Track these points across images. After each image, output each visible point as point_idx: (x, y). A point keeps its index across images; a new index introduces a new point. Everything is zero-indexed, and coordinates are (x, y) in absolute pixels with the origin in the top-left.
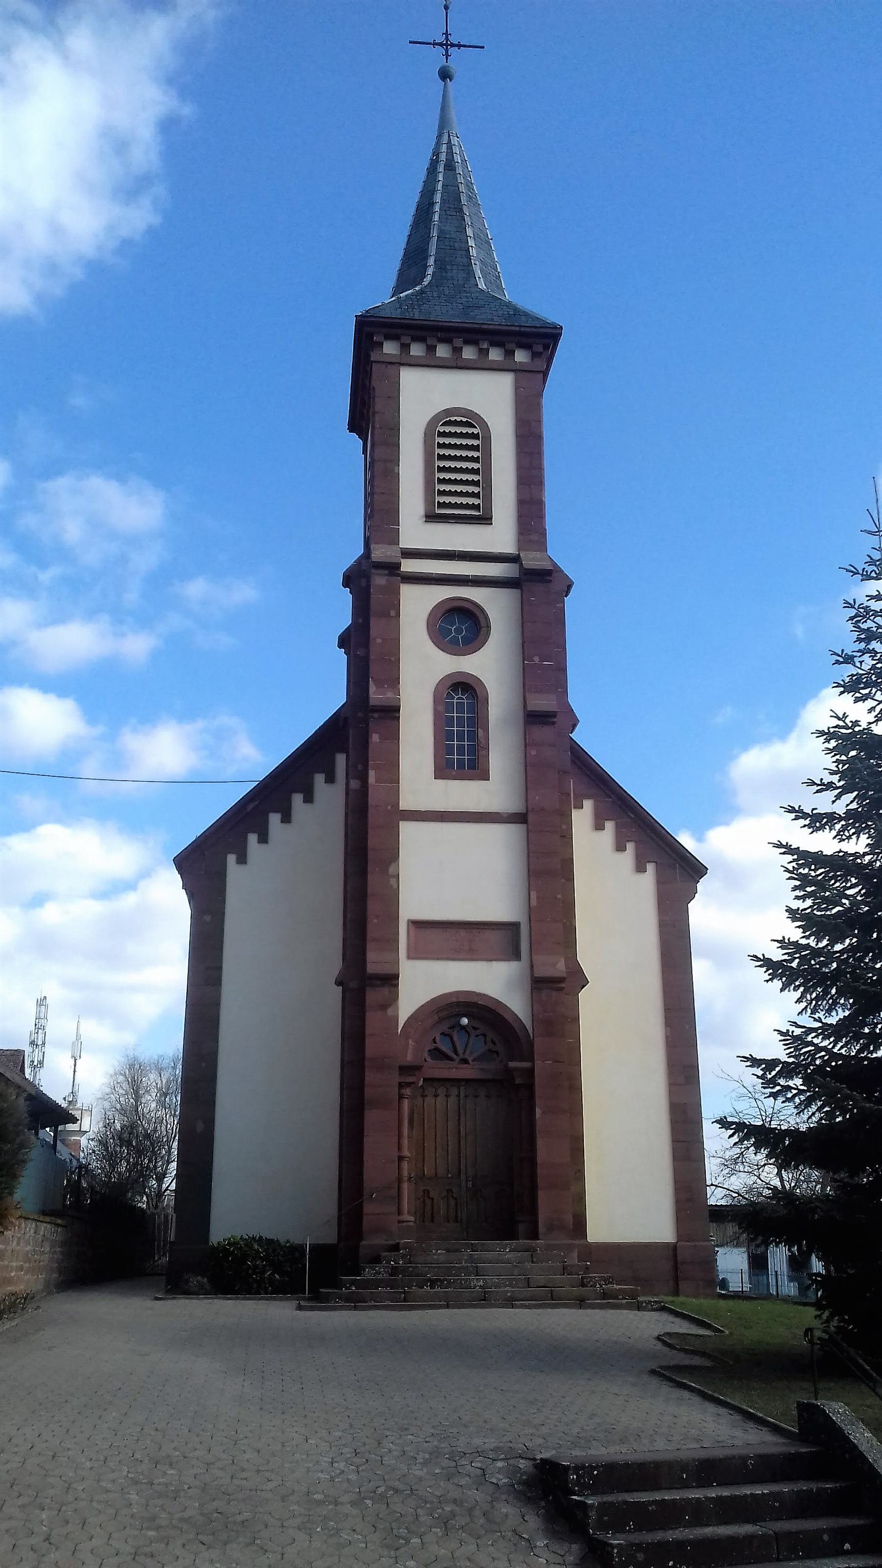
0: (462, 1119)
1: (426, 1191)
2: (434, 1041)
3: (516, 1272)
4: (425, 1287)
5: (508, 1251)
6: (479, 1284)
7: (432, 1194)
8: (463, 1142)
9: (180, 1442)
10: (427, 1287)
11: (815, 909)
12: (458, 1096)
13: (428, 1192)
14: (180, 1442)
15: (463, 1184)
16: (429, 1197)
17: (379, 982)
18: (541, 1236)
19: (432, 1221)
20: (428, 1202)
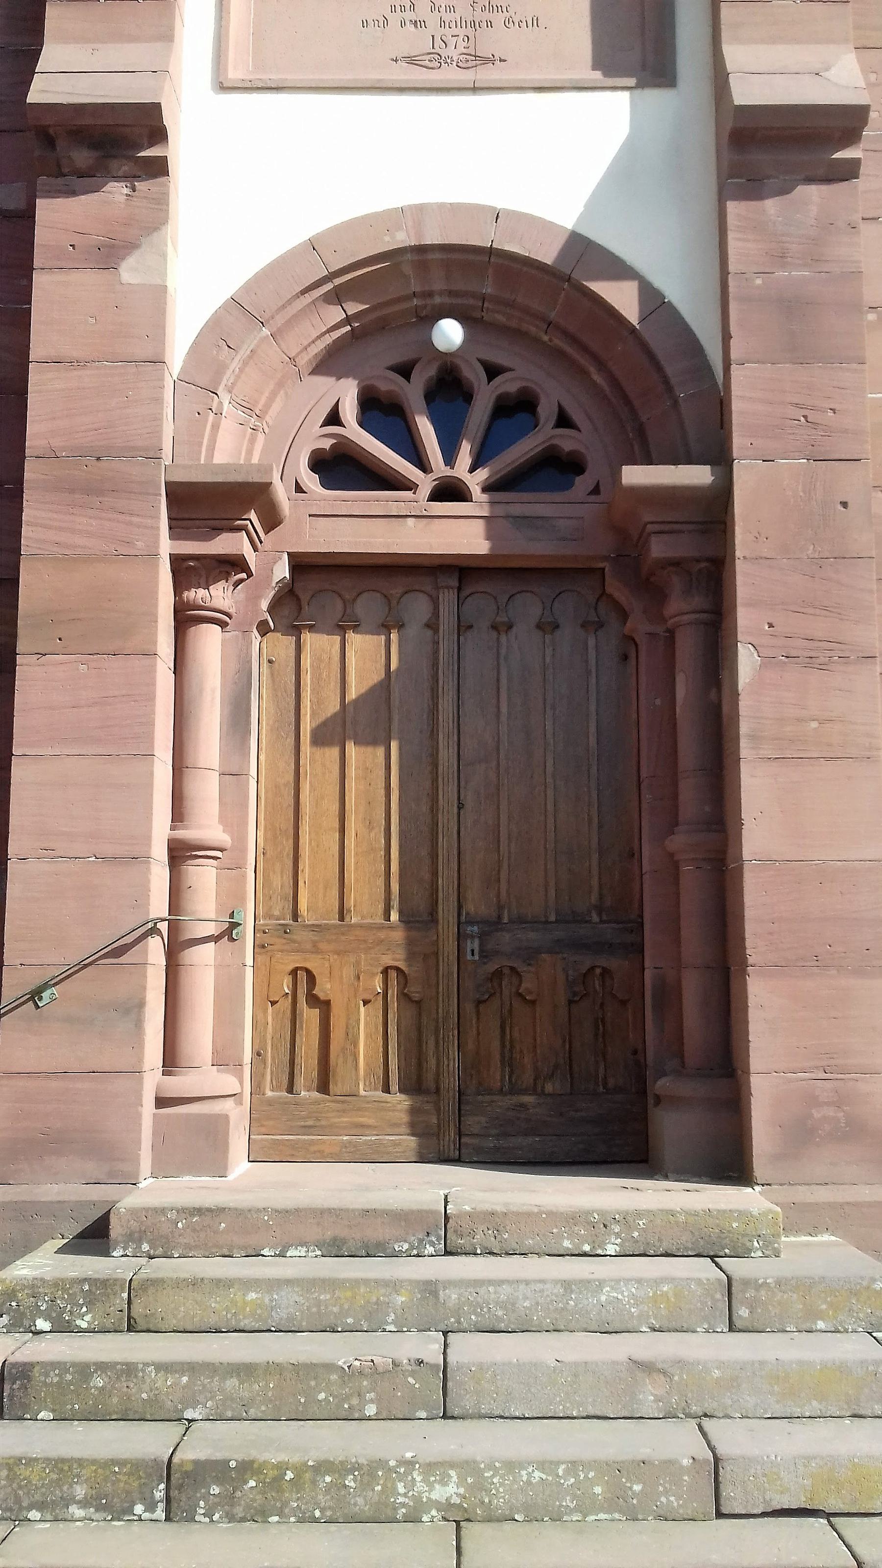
0: (446, 705)
1: (302, 976)
2: (334, 418)
3: (648, 1403)
4: (139, 1509)
5: (611, 1249)
6: (440, 1493)
7: (324, 988)
8: (447, 794)
9: (428, 1183)
10: (151, 1507)
11: (605, 1078)
12: (432, 625)
13: (311, 978)
14: (428, 1183)
15: (450, 947)
16: (313, 1000)
17: (82, 157)
18: (760, 1167)
19: (324, 1087)
20: (310, 1016)
